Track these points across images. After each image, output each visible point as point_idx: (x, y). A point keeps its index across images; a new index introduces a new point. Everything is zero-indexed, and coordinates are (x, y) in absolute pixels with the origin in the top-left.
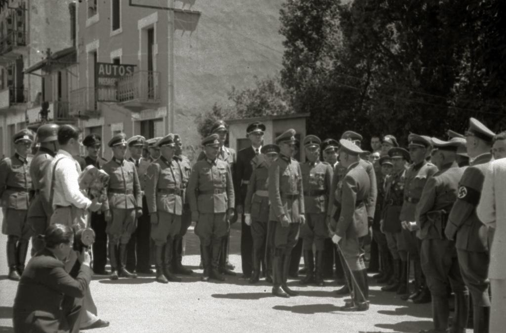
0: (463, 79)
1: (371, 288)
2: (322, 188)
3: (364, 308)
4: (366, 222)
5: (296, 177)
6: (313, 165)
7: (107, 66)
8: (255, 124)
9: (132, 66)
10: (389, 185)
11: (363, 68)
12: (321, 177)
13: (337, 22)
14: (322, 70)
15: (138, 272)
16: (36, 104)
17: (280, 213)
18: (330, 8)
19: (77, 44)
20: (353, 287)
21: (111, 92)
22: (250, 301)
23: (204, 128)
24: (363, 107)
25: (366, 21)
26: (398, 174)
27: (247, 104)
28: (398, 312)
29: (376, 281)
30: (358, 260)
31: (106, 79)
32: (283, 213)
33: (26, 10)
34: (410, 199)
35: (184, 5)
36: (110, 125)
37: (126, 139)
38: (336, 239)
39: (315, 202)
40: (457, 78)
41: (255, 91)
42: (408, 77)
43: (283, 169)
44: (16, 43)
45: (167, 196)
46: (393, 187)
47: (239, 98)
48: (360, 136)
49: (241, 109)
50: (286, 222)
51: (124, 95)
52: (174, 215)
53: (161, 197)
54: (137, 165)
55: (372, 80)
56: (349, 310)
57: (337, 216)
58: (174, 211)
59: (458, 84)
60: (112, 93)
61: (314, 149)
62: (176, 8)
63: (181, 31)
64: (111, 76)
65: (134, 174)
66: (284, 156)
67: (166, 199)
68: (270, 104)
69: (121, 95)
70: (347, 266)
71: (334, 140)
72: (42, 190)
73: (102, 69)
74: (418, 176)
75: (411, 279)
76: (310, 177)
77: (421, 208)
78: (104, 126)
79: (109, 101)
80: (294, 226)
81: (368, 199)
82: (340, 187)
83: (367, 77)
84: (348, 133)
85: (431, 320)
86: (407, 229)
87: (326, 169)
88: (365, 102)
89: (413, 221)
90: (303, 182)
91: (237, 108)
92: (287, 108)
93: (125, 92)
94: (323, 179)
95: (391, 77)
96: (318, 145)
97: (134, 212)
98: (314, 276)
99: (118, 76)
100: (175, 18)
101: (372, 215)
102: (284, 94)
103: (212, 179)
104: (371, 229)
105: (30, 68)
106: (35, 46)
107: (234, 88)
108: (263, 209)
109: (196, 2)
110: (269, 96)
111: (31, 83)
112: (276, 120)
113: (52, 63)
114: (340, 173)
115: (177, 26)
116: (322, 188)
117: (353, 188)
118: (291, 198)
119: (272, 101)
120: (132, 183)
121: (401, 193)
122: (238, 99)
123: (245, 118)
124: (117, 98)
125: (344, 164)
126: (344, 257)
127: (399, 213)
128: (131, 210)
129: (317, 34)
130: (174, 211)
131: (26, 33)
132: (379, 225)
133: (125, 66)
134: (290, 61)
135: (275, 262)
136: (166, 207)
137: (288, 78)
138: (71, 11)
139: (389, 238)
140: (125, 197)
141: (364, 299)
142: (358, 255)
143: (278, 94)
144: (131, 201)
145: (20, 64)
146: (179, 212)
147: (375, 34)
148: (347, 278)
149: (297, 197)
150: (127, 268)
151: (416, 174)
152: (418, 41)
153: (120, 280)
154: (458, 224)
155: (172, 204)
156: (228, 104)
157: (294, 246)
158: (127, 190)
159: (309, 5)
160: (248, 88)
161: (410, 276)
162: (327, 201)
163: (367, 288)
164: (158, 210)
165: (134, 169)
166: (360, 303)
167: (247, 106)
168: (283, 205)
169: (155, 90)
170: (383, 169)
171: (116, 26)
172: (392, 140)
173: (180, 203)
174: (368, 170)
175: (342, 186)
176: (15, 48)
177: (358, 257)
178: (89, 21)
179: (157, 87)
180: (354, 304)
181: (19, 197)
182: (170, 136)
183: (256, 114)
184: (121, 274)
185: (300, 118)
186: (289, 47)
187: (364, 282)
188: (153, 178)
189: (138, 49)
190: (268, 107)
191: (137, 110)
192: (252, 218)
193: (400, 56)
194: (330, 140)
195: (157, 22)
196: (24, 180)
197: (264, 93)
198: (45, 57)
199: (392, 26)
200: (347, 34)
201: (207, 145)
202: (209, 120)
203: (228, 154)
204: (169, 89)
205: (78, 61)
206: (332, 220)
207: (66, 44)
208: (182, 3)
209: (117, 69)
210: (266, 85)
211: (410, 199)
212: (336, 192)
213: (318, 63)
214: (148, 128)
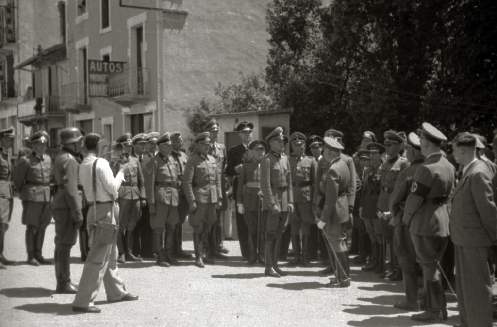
0: (434, 76)
1: (352, 268)
2: (308, 180)
3: (347, 285)
4: (347, 209)
5: (285, 171)
6: (299, 158)
7: (97, 63)
8: (244, 124)
9: (122, 63)
10: (367, 176)
11: (343, 65)
12: (307, 170)
13: (317, 23)
14: (306, 67)
15: (141, 256)
16: (27, 99)
17: (271, 203)
18: (312, 9)
19: (67, 41)
20: (336, 266)
21: (102, 88)
22: (245, 280)
23: (193, 122)
24: (342, 102)
25: (345, 24)
26: (375, 166)
27: (233, 99)
28: (376, 288)
29: (356, 262)
30: (341, 243)
31: (97, 75)
32: (274, 202)
33: (16, 7)
34: (386, 189)
35: (172, 5)
36: (100, 119)
37: (131, 138)
38: (321, 225)
39: (302, 192)
40: (429, 76)
41: (240, 87)
42: (385, 75)
43: (273, 164)
44: (5, 40)
45: (165, 189)
46: (370, 178)
47: (225, 93)
48: (342, 134)
49: (227, 103)
50: (277, 211)
51: (117, 90)
52: (170, 206)
53: (159, 189)
54: (140, 160)
55: (351, 76)
56: (334, 287)
57: (321, 205)
58: (171, 202)
59: (429, 82)
60: (103, 88)
61: (300, 145)
62: (164, 8)
63: (170, 30)
64: (102, 72)
65: (138, 169)
66: (274, 152)
67: (162, 191)
68: (255, 98)
69: (114, 90)
70: (330, 247)
71: (319, 137)
72: (65, 185)
73: (93, 66)
74: (393, 169)
75: (388, 260)
76: (296, 169)
77: (395, 198)
78: (95, 119)
79: (100, 96)
80: (283, 215)
81: (349, 189)
82: (325, 179)
83: (346, 74)
84: (330, 131)
85: (404, 294)
86: (382, 219)
87: (311, 162)
88: (344, 97)
89: (387, 211)
90: (292, 175)
91: (223, 102)
92: (271, 102)
93: (116, 88)
94: (309, 172)
95: (368, 74)
96: (304, 141)
97: (138, 203)
98: (301, 258)
99: (108, 72)
100: (163, 17)
101: (353, 203)
102: (268, 89)
103: (208, 172)
104: (351, 215)
105: (21, 64)
106: (25, 42)
107: (220, 84)
108: (252, 199)
109: (184, 2)
110: (254, 91)
111: (21, 77)
112: (261, 115)
113: (43, 59)
114: (324, 167)
115: (166, 25)
116: (308, 180)
117: (335, 180)
118: (282, 189)
119: (257, 96)
120: (136, 178)
121: (378, 183)
122: (224, 94)
123: (232, 113)
124: (108, 94)
125: (327, 159)
126: (329, 242)
127: (376, 201)
128: (136, 200)
129: (300, 34)
130: (171, 202)
131: (16, 30)
132: (359, 212)
133: (115, 63)
134: (275, 58)
135: (267, 246)
136: (164, 200)
137: (273, 74)
138: (60, 10)
139: (367, 223)
140: (131, 189)
141: (347, 277)
142: (340, 239)
143: (263, 89)
144: (136, 193)
145: (10, 59)
146: (175, 203)
147: (353, 35)
148: (331, 258)
149: (287, 188)
150: (133, 253)
151: (391, 167)
152: (394, 40)
153: (128, 264)
154: (412, 213)
155: (169, 196)
156: (214, 99)
157: (284, 231)
158: (132, 183)
159: (293, 7)
160: (233, 84)
161: (387, 258)
162: (312, 191)
163: (349, 268)
164: (156, 201)
165: (138, 164)
166: (342, 280)
167: (233, 101)
168: (274, 195)
169: (144, 86)
170: (361, 162)
171: (106, 24)
172: (372, 136)
173: (176, 194)
174: (348, 164)
175: (326, 178)
176: (6, 44)
177: (340, 240)
178: (78, 20)
179: (146, 83)
180: (338, 281)
181: (37, 191)
182: (166, 135)
183: (242, 109)
184: (128, 258)
185: (286, 113)
186: (274, 45)
187: (347, 264)
188: (152, 173)
189: (127, 47)
190: (253, 102)
191: (127, 104)
192: (245, 208)
193: (377, 54)
194: (315, 136)
195: (146, 22)
196: (41, 176)
197: (249, 88)
198: (36, 53)
199: (368, 26)
200: (326, 35)
201: (199, 142)
202: (198, 114)
203: (219, 149)
204: (159, 84)
205: (68, 56)
206: (318, 208)
207: (54, 40)
208: (170, 3)
209: (108, 66)
210: (251, 80)
211: (386, 189)
212: (321, 184)
213: (301, 61)
214: (137, 123)
